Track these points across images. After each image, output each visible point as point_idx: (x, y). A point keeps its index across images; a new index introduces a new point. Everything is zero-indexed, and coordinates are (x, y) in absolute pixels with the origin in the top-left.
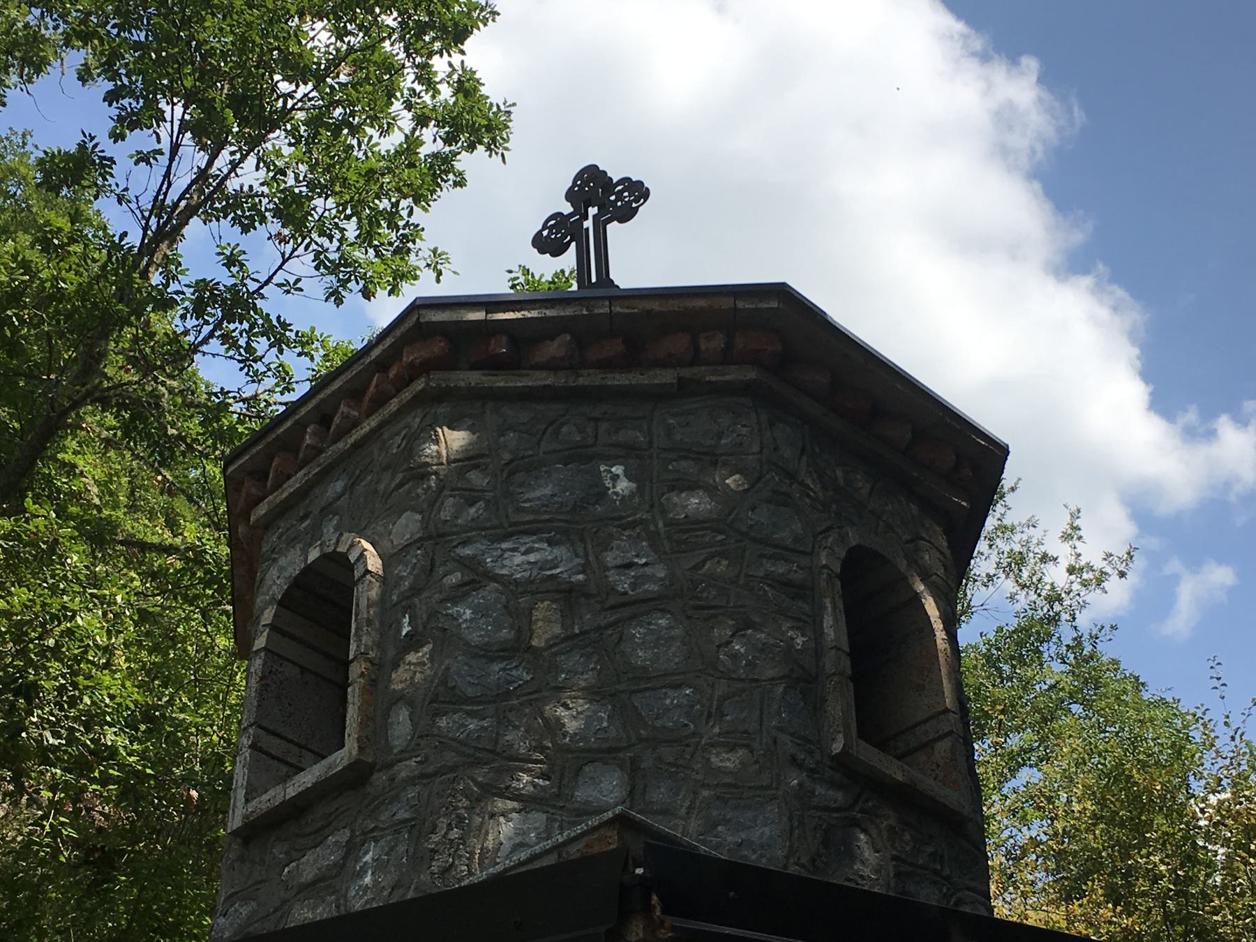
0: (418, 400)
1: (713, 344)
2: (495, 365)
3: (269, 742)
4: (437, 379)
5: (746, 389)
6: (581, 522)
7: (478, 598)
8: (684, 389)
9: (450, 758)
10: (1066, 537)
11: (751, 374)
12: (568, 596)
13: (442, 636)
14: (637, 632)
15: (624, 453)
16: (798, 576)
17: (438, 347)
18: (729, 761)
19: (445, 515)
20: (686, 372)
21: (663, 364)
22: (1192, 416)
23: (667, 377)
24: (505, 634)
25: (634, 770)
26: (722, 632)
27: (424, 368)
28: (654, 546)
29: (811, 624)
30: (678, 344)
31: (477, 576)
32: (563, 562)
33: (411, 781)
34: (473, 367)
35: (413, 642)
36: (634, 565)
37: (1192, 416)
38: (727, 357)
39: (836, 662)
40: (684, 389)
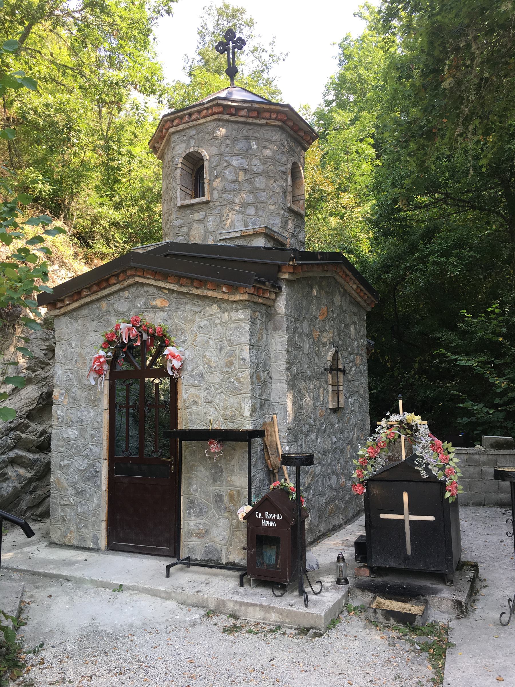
0: (215, 120)
1: (274, 116)
2: (231, 114)
3: (183, 188)
4: (220, 116)
5: (278, 126)
6: (246, 154)
7: (229, 169)
8: (267, 125)
9: (226, 203)
10: (271, 44)
11: (280, 123)
12: (245, 171)
13: (223, 178)
14: (257, 179)
15: (256, 139)
16: (285, 170)
17: (221, 109)
18: (272, 208)
19: (222, 150)
20: (268, 121)
21: (264, 119)
22: (336, 81)
23: (264, 122)
24: (235, 178)
25: (256, 207)
26: (272, 182)
27: (218, 113)
28: (260, 161)
29: (286, 180)
30: (267, 115)
31: (229, 165)
32: (244, 163)
33: (219, 206)
34: (228, 114)
35: (217, 177)
36: (258, 166)
37: (336, 81)
38: (276, 119)
39: (289, 188)
40: (267, 125)
